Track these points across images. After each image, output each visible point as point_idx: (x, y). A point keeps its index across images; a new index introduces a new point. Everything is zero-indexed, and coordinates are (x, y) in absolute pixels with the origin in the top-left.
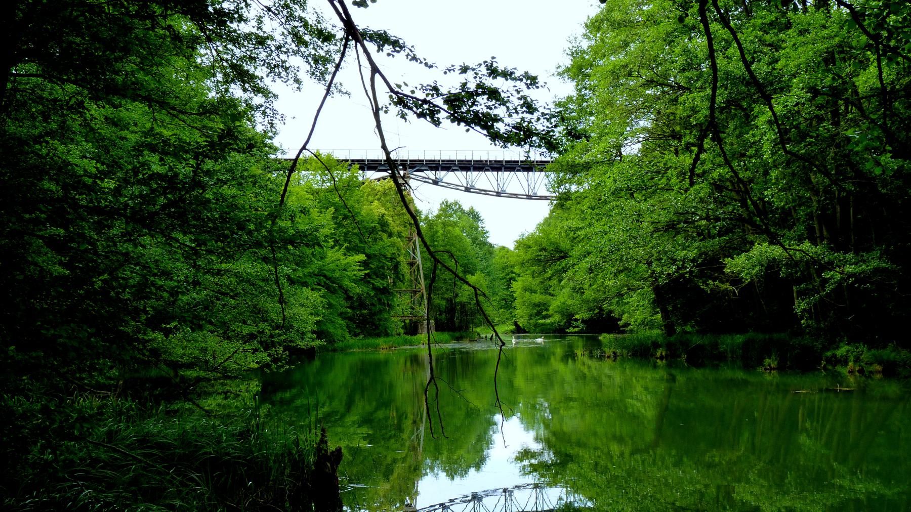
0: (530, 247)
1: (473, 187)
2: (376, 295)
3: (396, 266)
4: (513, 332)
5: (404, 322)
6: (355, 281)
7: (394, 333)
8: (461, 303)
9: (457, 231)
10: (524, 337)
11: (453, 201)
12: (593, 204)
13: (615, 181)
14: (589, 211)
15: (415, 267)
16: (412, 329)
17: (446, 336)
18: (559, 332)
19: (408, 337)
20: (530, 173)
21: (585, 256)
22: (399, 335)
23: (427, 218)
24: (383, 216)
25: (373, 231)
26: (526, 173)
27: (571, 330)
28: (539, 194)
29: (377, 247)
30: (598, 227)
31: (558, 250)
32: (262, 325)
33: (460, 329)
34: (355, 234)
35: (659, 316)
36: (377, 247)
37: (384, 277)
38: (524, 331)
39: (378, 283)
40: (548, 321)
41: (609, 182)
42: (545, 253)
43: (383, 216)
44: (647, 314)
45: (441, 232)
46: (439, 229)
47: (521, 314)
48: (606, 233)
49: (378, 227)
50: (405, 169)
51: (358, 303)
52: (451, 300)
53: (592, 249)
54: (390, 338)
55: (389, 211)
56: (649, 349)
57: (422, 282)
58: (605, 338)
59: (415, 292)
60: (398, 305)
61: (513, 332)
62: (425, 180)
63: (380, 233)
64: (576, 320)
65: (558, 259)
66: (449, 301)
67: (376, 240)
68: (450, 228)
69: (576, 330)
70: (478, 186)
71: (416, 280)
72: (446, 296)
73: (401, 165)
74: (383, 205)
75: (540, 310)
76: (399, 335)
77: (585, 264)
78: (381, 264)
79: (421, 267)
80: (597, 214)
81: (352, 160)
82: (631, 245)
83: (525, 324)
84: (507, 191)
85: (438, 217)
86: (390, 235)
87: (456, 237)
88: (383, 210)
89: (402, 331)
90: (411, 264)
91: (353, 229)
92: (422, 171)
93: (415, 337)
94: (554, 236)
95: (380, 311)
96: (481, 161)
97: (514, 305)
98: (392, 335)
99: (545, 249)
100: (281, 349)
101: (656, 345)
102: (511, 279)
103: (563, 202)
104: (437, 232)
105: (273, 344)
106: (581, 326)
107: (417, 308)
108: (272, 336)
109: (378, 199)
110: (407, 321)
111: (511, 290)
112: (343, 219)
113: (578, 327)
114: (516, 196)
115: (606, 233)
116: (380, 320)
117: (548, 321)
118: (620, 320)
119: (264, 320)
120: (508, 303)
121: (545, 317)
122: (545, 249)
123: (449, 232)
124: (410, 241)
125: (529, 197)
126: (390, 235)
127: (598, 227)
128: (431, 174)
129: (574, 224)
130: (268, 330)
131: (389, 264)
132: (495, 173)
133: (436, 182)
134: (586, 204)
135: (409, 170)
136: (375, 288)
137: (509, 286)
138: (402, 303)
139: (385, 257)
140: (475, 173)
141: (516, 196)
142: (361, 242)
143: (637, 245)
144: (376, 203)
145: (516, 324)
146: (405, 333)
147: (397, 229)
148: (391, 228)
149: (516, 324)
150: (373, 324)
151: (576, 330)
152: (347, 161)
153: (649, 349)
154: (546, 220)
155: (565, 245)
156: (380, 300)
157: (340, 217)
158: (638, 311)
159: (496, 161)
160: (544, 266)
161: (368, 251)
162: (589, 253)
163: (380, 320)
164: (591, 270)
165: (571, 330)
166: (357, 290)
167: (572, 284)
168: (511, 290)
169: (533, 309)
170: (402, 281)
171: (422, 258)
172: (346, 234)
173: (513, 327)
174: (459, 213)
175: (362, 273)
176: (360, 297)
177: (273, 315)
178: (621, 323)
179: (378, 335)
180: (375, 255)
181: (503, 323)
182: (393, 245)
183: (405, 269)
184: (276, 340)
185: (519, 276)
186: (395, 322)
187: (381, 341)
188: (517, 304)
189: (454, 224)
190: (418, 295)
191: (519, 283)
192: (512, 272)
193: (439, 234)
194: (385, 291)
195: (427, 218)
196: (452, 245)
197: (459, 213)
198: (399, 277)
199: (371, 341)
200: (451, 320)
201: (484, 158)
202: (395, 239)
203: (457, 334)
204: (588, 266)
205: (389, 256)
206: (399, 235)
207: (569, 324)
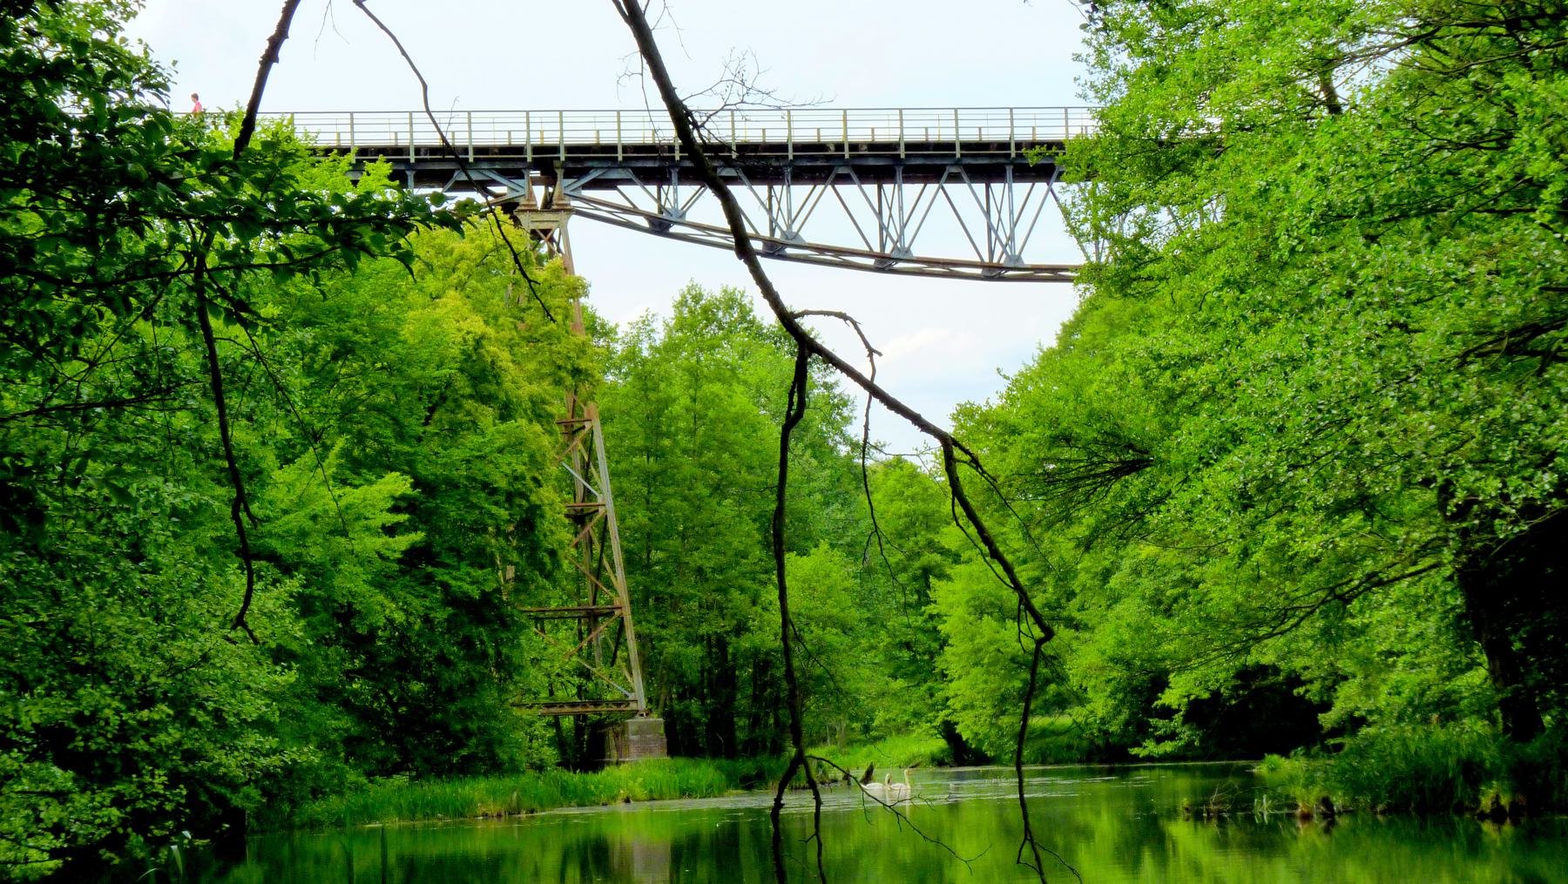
0: (1014, 431)
1: (793, 240)
2: (452, 625)
3: (528, 523)
4: (939, 762)
5: (556, 724)
6: (381, 582)
7: (521, 757)
8: (756, 652)
9: (740, 400)
10: (984, 776)
11: (718, 294)
12: (1241, 269)
13: (1323, 180)
14: (1229, 295)
15: (591, 528)
16: (588, 747)
17: (705, 771)
18: (1108, 755)
19: (575, 778)
20: (997, 187)
21: (1223, 450)
22: (540, 768)
23: (632, 355)
24: (478, 343)
25: (439, 398)
26: (980, 188)
27: (1150, 747)
28: (1029, 259)
29: (457, 454)
30: (1268, 346)
31: (1114, 439)
32: (91, 695)
33: (752, 748)
34: (380, 409)
35: (1478, 677)
36: (457, 454)
37: (482, 559)
38: (980, 759)
39: (466, 580)
40: (1064, 720)
41: (1304, 188)
42: (1067, 453)
43: (478, 343)
44: (1431, 674)
45: (685, 401)
46: (676, 390)
47: (969, 695)
48: (1295, 362)
49: (463, 385)
50: (549, 179)
51: (385, 658)
52: (721, 643)
53: (1245, 421)
54: (508, 782)
55: (499, 328)
56: (1449, 784)
57: (620, 579)
58: (1278, 768)
59: (593, 617)
60: (535, 661)
61: (939, 762)
62: (621, 218)
63: (469, 404)
64: (1167, 712)
65: (1117, 473)
66: (718, 644)
67: (455, 430)
68: (717, 388)
69: (1168, 747)
70: (812, 234)
71: (598, 572)
72: (704, 629)
73: (536, 165)
74: (480, 307)
75: (1037, 679)
76: (540, 768)
77: (1221, 479)
78: (473, 516)
79: (613, 526)
80: (1258, 306)
81: (363, 151)
82: (1390, 402)
83: (983, 730)
84: (917, 252)
85: (671, 348)
86: (506, 412)
87: (736, 420)
88: (477, 325)
89: (550, 754)
90: (579, 519)
91: (373, 391)
92: (610, 184)
93: (592, 778)
94: (1099, 386)
95: (471, 686)
96: (821, 147)
97: (940, 663)
98: (515, 770)
99: (1068, 439)
100: (159, 780)
101: (1473, 772)
102: (927, 572)
103: (1126, 276)
104: (668, 402)
105: (130, 764)
106: (1186, 733)
107: (600, 670)
108: (124, 733)
109: (460, 286)
110: (567, 723)
111: (931, 609)
112: (335, 357)
113: (1172, 736)
114: (947, 269)
115: (1295, 362)
116: (465, 715)
117: (1064, 720)
118: (1326, 706)
119: (98, 672)
120: (919, 660)
121: (1061, 703)
122: (1068, 439)
123: (712, 401)
124: (572, 433)
125: (993, 272)
126: (506, 412)
127: (1268, 346)
128: (642, 196)
129: (1174, 345)
130: (112, 711)
131: (503, 513)
132: (871, 189)
133: (659, 226)
134: (1209, 279)
135: (564, 184)
136: (453, 599)
137: (924, 598)
138: (549, 652)
139: (489, 489)
140: (800, 191)
141: (947, 269)
142: (401, 437)
143: (1409, 401)
144: (452, 298)
145: (949, 731)
146: (564, 764)
147: (527, 390)
148: (508, 385)
149: (949, 731)
150: (448, 734)
151: (1168, 747)
152: (344, 151)
153: (1449, 784)
154: (1048, 357)
155: (1141, 420)
156: (467, 643)
157: (326, 350)
158: (1404, 663)
159: (873, 146)
160: (1067, 500)
161: (423, 470)
162: (1236, 439)
163: (465, 715)
164: (1244, 501)
165: (1150, 747)
166: (386, 611)
167: (1147, 584)
168: (931, 609)
169: (1010, 676)
170: (548, 576)
171: (619, 494)
172: (347, 412)
173: (939, 744)
174: (741, 338)
175: (403, 542)
176: (402, 638)
177: (131, 659)
178: (1327, 720)
179: (466, 769)
180: (453, 485)
181: (903, 729)
182: (516, 446)
183: (557, 532)
184: (141, 745)
185: (957, 558)
186: (529, 728)
187: (476, 790)
188: (951, 659)
189: (728, 375)
190: (604, 628)
191: (958, 585)
192: (931, 546)
193: (676, 409)
194: (482, 610)
195: (632, 355)
196: (724, 446)
197: (741, 338)
198: (537, 558)
199: (437, 789)
200: (721, 720)
201: (832, 135)
202: (520, 424)
203: (746, 766)
204: (1236, 481)
205: (502, 483)
206: (538, 412)
207: (1139, 729)
